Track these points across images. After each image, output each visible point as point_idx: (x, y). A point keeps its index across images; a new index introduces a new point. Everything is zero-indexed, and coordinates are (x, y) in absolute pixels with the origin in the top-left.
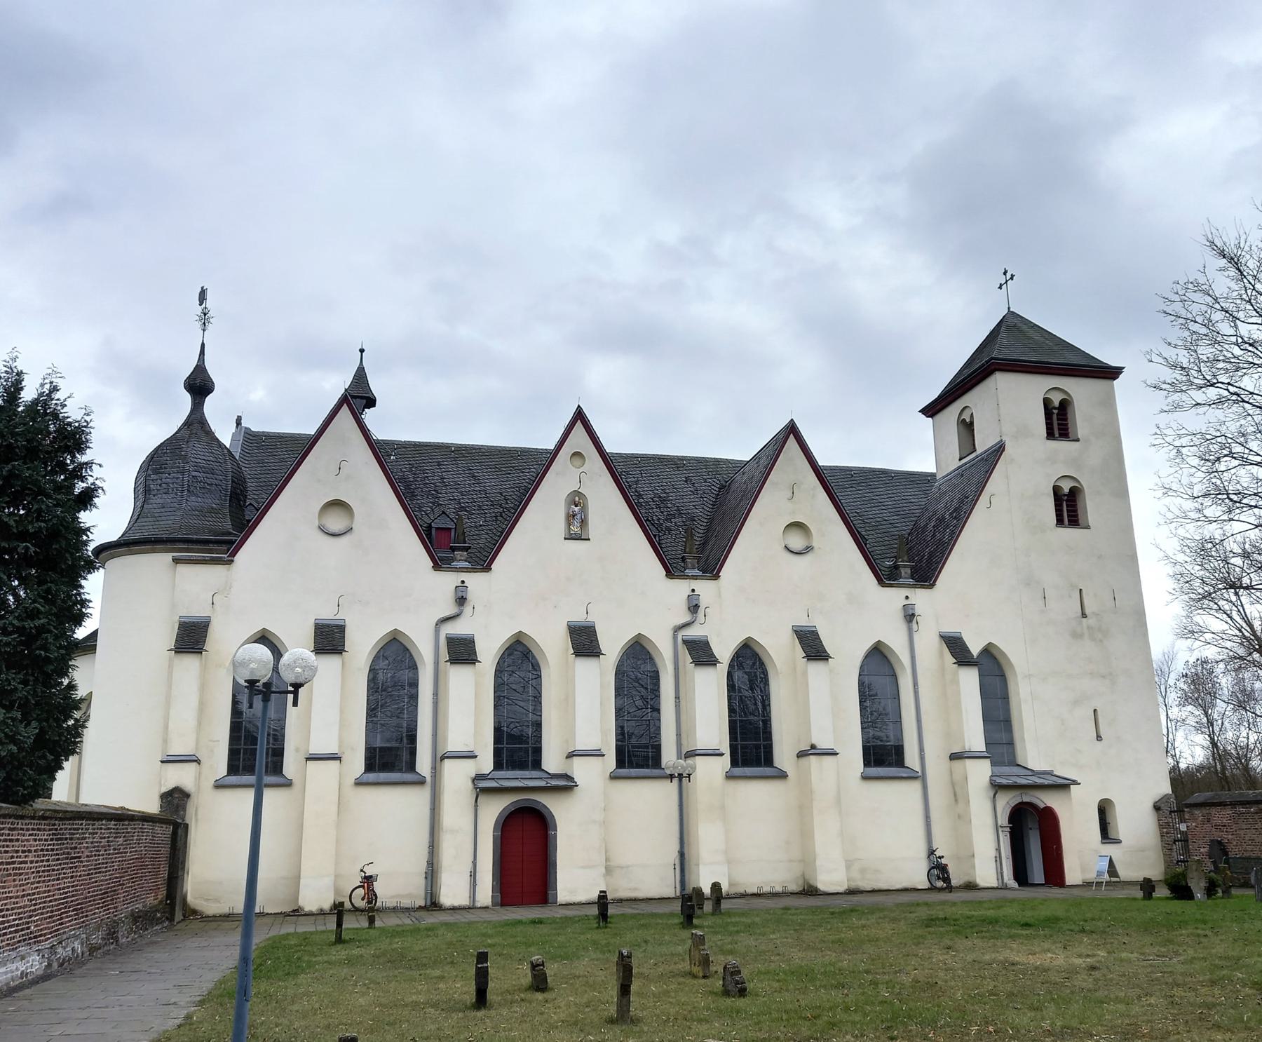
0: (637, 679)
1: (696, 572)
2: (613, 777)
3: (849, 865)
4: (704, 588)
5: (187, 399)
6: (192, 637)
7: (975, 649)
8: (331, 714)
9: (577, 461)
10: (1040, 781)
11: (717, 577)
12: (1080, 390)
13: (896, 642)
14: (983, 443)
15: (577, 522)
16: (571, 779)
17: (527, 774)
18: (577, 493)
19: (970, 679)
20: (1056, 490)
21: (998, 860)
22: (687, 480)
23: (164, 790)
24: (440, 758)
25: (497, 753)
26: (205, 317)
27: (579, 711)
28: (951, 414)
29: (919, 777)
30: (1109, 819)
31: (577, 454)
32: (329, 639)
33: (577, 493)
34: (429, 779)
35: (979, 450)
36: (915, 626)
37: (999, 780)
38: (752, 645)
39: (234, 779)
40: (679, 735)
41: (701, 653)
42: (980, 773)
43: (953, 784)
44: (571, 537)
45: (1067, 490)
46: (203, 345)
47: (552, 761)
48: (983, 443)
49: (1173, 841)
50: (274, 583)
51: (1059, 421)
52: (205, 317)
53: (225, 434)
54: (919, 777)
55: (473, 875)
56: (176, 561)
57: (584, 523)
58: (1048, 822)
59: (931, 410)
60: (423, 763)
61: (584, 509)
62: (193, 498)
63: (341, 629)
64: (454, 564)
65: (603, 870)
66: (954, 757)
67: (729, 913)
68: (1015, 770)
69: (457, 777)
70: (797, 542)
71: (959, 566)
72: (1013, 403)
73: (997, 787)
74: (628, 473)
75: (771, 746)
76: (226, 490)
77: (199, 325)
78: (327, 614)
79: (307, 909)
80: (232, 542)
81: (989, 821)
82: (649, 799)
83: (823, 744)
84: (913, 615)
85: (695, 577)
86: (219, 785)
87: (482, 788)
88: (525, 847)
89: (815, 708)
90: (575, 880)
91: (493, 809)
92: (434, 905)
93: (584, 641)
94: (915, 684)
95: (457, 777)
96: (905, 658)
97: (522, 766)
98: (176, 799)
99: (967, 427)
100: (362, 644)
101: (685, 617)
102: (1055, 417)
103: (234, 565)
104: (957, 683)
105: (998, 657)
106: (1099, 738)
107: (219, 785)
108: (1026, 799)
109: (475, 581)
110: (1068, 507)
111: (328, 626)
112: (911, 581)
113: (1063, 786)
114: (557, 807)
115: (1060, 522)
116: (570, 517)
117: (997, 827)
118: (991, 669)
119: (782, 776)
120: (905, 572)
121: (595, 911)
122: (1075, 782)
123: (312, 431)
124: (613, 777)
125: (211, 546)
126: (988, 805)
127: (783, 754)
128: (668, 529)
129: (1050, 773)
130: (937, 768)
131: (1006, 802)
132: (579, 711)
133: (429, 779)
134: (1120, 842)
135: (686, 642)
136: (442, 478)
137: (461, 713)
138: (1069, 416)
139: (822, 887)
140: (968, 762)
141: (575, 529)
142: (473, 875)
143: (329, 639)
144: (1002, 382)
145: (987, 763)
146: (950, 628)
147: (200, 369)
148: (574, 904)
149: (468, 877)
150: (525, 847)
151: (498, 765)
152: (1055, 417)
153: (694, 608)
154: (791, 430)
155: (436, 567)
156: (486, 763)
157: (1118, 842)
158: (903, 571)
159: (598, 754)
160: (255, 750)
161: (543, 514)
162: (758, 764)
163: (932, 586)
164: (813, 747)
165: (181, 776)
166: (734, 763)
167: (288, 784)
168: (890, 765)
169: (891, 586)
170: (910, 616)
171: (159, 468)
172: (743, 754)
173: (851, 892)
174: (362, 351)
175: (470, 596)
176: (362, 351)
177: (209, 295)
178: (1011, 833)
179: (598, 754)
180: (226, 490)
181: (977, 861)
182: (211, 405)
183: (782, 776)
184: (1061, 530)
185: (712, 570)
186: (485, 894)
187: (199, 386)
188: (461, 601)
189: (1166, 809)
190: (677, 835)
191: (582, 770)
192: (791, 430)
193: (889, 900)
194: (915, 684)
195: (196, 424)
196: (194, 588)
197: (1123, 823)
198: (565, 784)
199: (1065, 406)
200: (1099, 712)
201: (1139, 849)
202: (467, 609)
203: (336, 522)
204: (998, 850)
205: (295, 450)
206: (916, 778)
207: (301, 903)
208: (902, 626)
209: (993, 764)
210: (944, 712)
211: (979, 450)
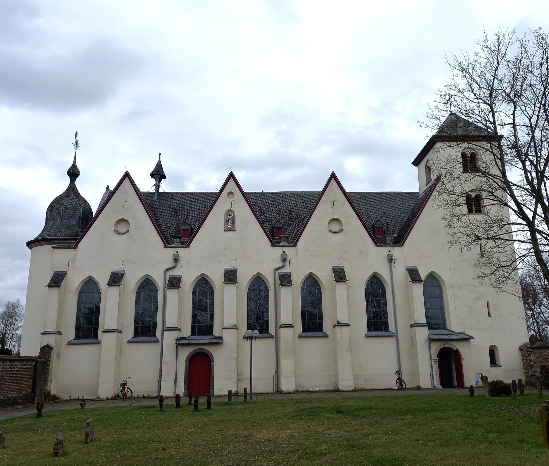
0: (258, 291)
1: (286, 243)
2: (300, 337)
3: (355, 377)
7: (423, 275)
8: (117, 310)
9: (231, 196)
11: (295, 245)
15: (230, 223)
17: (205, 337)
18: (230, 210)
19: (418, 290)
21: (432, 375)
22: (304, 202)
23: (42, 346)
24: (164, 330)
26: (76, 145)
27: (230, 307)
28: (423, 164)
31: (231, 193)
33: (230, 210)
34: (160, 340)
36: (393, 264)
37: (431, 337)
38: (313, 275)
39: (136, 339)
40: (276, 318)
42: (423, 333)
43: (412, 338)
45: (473, 196)
46: (75, 156)
49: (527, 365)
51: (470, 163)
52: (76, 145)
55: (175, 382)
57: (233, 224)
59: (416, 163)
60: (272, 331)
61: (234, 216)
62: (65, 221)
65: (236, 380)
67: (254, 403)
68: (445, 332)
69: (170, 338)
70: (335, 227)
71: (415, 236)
73: (431, 340)
74: (356, 201)
76: (80, 217)
77: (73, 148)
79: (101, 397)
80: (76, 239)
81: (428, 356)
83: (344, 321)
85: (285, 246)
86: (129, 342)
87: (181, 343)
88: (200, 368)
89: (345, 305)
90: (223, 383)
91: (185, 353)
92: (279, 391)
94: (393, 292)
95: (170, 338)
96: (388, 280)
97: (204, 333)
98: (46, 350)
100: (132, 281)
103: (78, 249)
104: (412, 290)
105: (436, 276)
106: (490, 315)
107: (69, 344)
108: (447, 346)
109: (183, 252)
111: (117, 274)
112: (392, 243)
113: (467, 339)
114: (214, 352)
116: (227, 221)
119: (326, 336)
121: (174, 402)
122: (472, 338)
123: (320, 190)
124: (300, 337)
126: (427, 349)
127: (327, 326)
128: (291, 225)
129: (463, 333)
130: (403, 331)
131: (436, 347)
132: (230, 307)
133: (160, 340)
134: (501, 366)
135: (280, 276)
136: (191, 207)
137: (175, 311)
139: (341, 388)
140: (416, 328)
141: (229, 226)
142: (175, 382)
143: (231, 277)
145: (426, 329)
146: (411, 265)
147: (74, 166)
148: (221, 396)
149: (174, 384)
150: (200, 368)
151: (193, 333)
154: (127, 175)
155: (273, 245)
156: (187, 331)
157: (500, 366)
159: (291, 326)
160: (88, 327)
161: (215, 219)
162: (316, 331)
163: (402, 245)
164: (338, 322)
165: (50, 340)
167: (326, 336)
168: (382, 330)
170: (390, 260)
172: (309, 326)
173: (355, 391)
174: (160, 154)
176: (160, 154)
180: (80, 217)
181: (421, 376)
182: (78, 183)
186: (181, 391)
187: (74, 173)
188: (176, 260)
189: (525, 350)
192: (127, 175)
193: (313, 396)
194: (393, 292)
195: (72, 190)
197: (502, 357)
198: (219, 342)
199: (474, 157)
200: (490, 303)
201: (510, 369)
202: (179, 264)
203: (122, 228)
204: (432, 370)
206: (393, 336)
207: (99, 395)
208: (387, 264)
209: (429, 329)
210: (407, 305)
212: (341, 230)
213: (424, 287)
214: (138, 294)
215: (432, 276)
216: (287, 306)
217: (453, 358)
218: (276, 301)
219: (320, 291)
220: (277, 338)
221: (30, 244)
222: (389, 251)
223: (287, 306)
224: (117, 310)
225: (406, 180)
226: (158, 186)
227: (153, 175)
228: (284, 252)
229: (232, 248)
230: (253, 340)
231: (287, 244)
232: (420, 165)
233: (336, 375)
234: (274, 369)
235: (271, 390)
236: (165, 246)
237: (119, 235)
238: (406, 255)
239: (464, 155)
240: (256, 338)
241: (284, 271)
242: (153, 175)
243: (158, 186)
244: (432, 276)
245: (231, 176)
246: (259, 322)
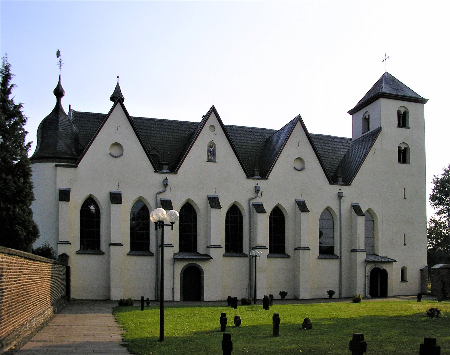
0: (234, 216)
2: (129, 254)
4: (262, 183)
6: (65, 195)
9: (212, 129)
10: (383, 260)
12: (411, 106)
13: (334, 207)
14: (373, 127)
16: (210, 256)
18: (212, 143)
20: (399, 148)
21: (365, 288)
25: (180, 245)
27: (214, 229)
28: (361, 113)
29: (339, 258)
31: (212, 126)
32: (116, 198)
33: (212, 143)
35: (371, 130)
36: (342, 200)
37: (368, 260)
38: (92, 197)
41: (260, 209)
42: (361, 257)
44: (209, 161)
45: (403, 149)
47: (201, 249)
48: (373, 127)
50: (92, 175)
51: (403, 120)
53: (66, 110)
54: (339, 258)
56: (56, 166)
57: (214, 155)
58: (384, 274)
59: (352, 112)
61: (215, 147)
63: (120, 195)
64: (163, 171)
66: (352, 251)
70: (116, 151)
72: (388, 110)
75: (270, 234)
77: (58, 67)
78: (115, 190)
81: (364, 274)
82: (237, 264)
84: (342, 196)
85: (258, 179)
89: (305, 232)
93: (214, 202)
99: (367, 120)
101: (253, 195)
102: (401, 118)
106: (405, 245)
108: (377, 267)
109: (171, 178)
110: (403, 155)
113: (390, 262)
114: (205, 267)
115: (400, 161)
117: (366, 276)
118: (371, 217)
119: (289, 257)
120: (340, 179)
122: (395, 261)
125: (69, 160)
131: (370, 268)
132: (214, 229)
133: (155, 254)
138: (407, 118)
141: (211, 158)
142: (173, 289)
144: (383, 102)
146: (355, 202)
147: (59, 85)
152: (401, 118)
153: (257, 191)
154: (213, 110)
158: (339, 179)
159: (220, 247)
161: (198, 150)
166: (270, 252)
167: (103, 253)
169: (334, 185)
170: (340, 196)
171: (48, 126)
174: (118, 77)
175: (169, 183)
176: (118, 77)
178: (370, 279)
179: (220, 247)
183: (289, 257)
184: (400, 164)
185: (264, 175)
187: (59, 93)
191: (213, 253)
192: (213, 110)
195: (58, 108)
196: (64, 177)
197: (409, 276)
198: (207, 258)
202: (168, 189)
204: (365, 285)
205: (99, 120)
211: (371, 130)
212: (303, 169)
215: (369, 211)
216: (260, 230)
217: (379, 276)
218: (250, 226)
222: (340, 189)
223: (260, 230)
225: (343, 127)
227: (112, 99)
228: (257, 184)
229: (211, 177)
231: (260, 177)
233: (108, 288)
234: (246, 282)
235: (171, 300)
236: (156, 171)
237: (116, 159)
238: (352, 193)
241: (258, 201)
242: (112, 99)
244: (369, 211)
246: (234, 243)
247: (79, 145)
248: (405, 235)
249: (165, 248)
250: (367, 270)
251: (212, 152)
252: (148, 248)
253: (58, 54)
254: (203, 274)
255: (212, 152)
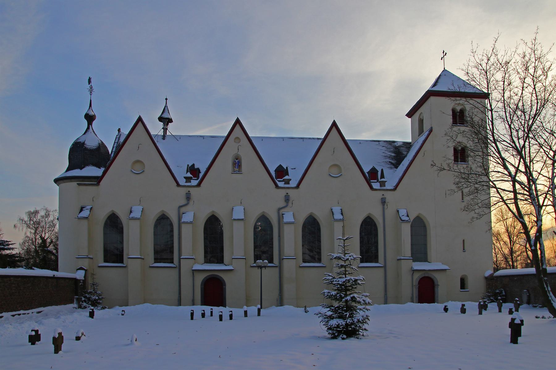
5: (85, 122)
12: (468, 105)
26: (91, 90)
28: (416, 116)
30: (73, 180)
31: (237, 138)
32: (35, 338)
36: (386, 206)
40: (280, 251)
51: (459, 117)
52: (91, 90)
59: (410, 115)
70: (334, 172)
77: (89, 93)
99: (421, 121)
113: (188, 165)
154: (140, 120)
170: (383, 202)
174: (166, 99)
176: (166, 99)
177: (92, 80)
190: (278, 288)
197: (470, 283)
199: (462, 112)
202: (191, 202)
204: (413, 295)
208: (380, 207)
213: (411, 227)
214: (156, 226)
216: (291, 242)
218: (279, 236)
219: (319, 229)
220: (280, 267)
221: (57, 181)
223: (291, 242)
224: (138, 242)
225: (403, 132)
226: (165, 130)
230: (263, 269)
232: (413, 117)
234: (277, 292)
239: (454, 111)
240: (265, 267)
243: (165, 130)
245: (238, 122)
247: (493, 190)
248: (464, 241)
249: (182, 260)
250: (414, 279)
251: (237, 164)
252: (155, 262)
253: (90, 81)
254: (225, 285)
255: (237, 164)
